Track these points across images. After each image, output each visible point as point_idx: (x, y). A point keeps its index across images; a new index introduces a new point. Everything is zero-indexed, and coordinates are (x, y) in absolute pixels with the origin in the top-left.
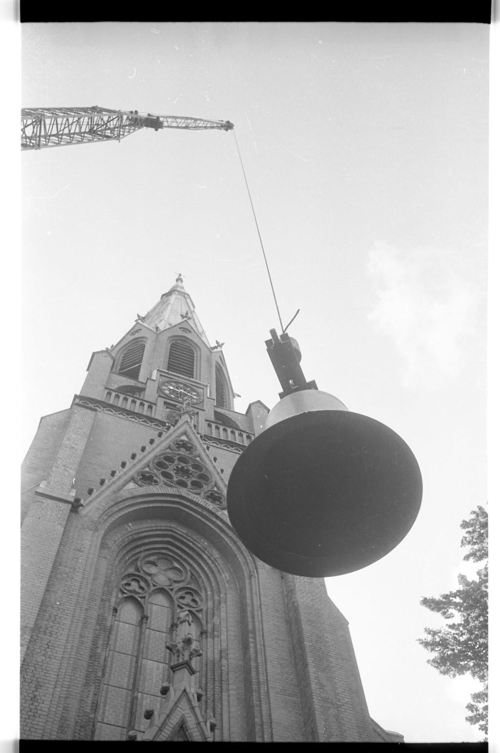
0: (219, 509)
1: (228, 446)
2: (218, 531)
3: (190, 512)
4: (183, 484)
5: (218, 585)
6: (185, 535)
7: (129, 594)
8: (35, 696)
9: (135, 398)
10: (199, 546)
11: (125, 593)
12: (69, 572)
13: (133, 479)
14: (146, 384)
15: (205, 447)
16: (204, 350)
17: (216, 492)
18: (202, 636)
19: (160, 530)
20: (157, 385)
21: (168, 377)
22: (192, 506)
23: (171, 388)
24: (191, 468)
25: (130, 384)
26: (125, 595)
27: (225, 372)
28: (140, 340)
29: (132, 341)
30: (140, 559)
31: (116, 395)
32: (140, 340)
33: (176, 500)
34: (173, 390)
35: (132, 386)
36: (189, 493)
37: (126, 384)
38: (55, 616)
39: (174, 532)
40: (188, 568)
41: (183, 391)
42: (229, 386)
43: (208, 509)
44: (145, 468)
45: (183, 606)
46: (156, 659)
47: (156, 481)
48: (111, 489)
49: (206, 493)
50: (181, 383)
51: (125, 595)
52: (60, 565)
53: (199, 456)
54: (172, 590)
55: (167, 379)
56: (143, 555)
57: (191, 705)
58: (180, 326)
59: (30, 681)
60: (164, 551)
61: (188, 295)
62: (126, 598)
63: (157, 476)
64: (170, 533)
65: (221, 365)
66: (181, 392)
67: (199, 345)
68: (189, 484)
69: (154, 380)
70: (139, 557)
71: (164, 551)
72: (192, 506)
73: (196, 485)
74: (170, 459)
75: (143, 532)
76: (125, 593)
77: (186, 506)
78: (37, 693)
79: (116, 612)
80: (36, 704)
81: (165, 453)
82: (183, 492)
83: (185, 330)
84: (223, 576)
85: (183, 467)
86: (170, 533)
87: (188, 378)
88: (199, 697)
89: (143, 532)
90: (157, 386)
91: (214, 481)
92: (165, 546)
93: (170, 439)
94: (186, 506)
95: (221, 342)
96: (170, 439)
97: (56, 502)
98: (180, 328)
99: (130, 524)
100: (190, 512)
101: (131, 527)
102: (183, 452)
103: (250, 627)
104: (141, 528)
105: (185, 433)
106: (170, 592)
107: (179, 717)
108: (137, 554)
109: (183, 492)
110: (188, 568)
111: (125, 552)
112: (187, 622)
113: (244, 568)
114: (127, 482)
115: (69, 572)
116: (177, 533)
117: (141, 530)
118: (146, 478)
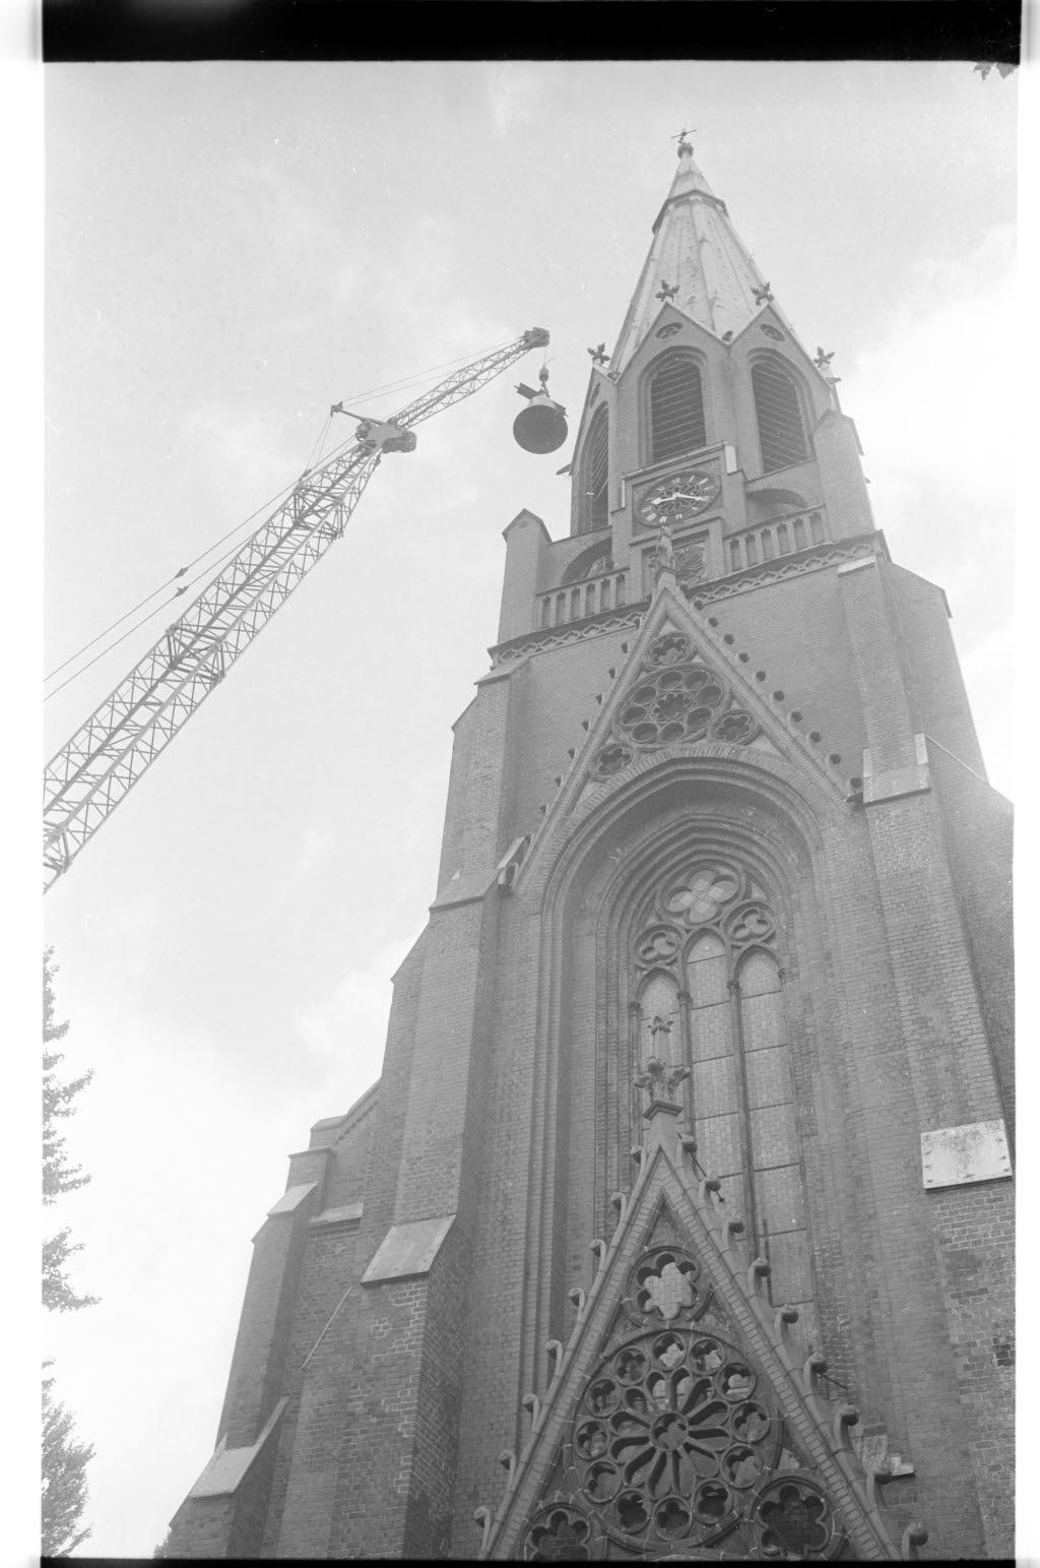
0: (742, 747)
1: (772, 573)
2: (753, 788)
3: (700, 778)
4: (673, 731)
6: (712, 817)
7: (651, 967)
8: (505, 1218)
9: (590, 580)
10: (740, 823)
11: (644, 969)
12: (518, 1005)
13: (587, 777)
16: (706, 347)
18: (89, 1451)
19: (670, 831)
20: (631, 513)
21: (641, 484)
22: (697, 767)
23: (657, 501)
25: (585, 548)
26: (645, 973)
28: (692, 353)
30: (658, 895)
31: (558, 597)
32: (692, 353)
33: (670, 770)
34: (662, 503)
35: (589, 549)
36: (685, 746)
37: (578, 552)
38: (510, 1086)
39: (696, 820)
40: (739, 867)
41: (679, 495)
43: (724, 759)
44: (607, 738)
45: (740, 944)
46: (713, 1056)
48: (554, 822)
50: (674, 477)
51: (645, 973)
52: (503, 1000)
55: (646, 487)
56: (659, 887)
59: (495, 1199)
60: (695, 859)
62: (647, 976)
63: (626, 746)
64: (691, 824)
66: (678, 498)
68: (685, 725)
70: (655, 895)
71: (695, 859)
72: (697, 767)
75: (643, 851)
76: (644, 969)
77: (687, 772)
78: (506, 1213)
80: (508, 1227)
82: (675, 749)
84: (790, 859)
86: (691, 824)
87: (684, 456)
89: (643, 851)
90: (630, 518)
91: (728, 691)
92: (693, 849)
93: (641, 650)
94: (687, 772)
96: (641, 650)
97: (461, 909)
99: (619, 850)
100: (700, 778)
101: (620, 855)
102: (669, 661)
104: (637, 847)
105: (666, 617)
106: (715, 928)
107: (656, 1194)
108: (649, 890)
109: (675, 749)
110: (739, 867)
114: (580, 789)
115: (518, 1005)
117: (638, 851)
118: (611, 758)
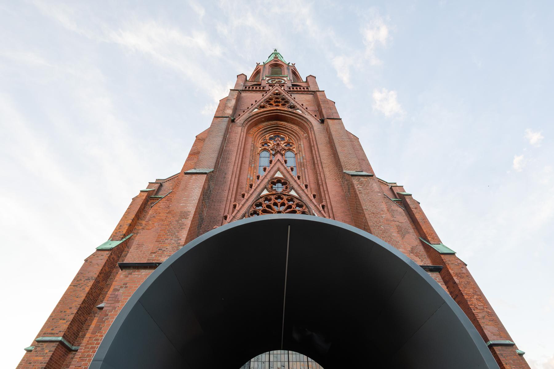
5: (299, 137)
14: (261, 82)
15: (289, 95)
17: (292, 105)
24: (281, 100)
27: (297, 74)
29: (256, 73)
42: (301, 79)
47: (266, 107)
49: (288, 106)
52: (230, 138)
53: (283, 96)
54: (281, 144)
57: (282, 163)
58: (273, 60)
61: (279, 53)
65: (295, 71)
67: (281, 64)
69: (264, 80)
73: (283, 105)
74: (271, 99)
79: (302, 214)
81: (269, 98)
83: (276, 61)
85: (277, 101)
88: (299, 177)
94: (278, 112)
95: (293, 63)
98: (274, 61)
103: (312, 145)
110: (286, 135)
111: (260, 137)
112: (243, 94)
113: (308, 127)
116: (279, 124)
